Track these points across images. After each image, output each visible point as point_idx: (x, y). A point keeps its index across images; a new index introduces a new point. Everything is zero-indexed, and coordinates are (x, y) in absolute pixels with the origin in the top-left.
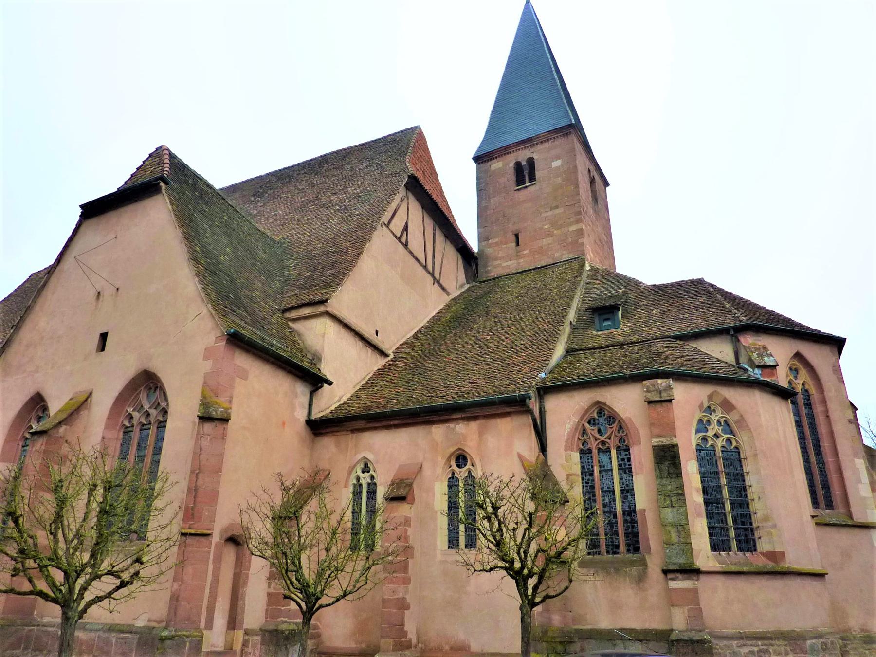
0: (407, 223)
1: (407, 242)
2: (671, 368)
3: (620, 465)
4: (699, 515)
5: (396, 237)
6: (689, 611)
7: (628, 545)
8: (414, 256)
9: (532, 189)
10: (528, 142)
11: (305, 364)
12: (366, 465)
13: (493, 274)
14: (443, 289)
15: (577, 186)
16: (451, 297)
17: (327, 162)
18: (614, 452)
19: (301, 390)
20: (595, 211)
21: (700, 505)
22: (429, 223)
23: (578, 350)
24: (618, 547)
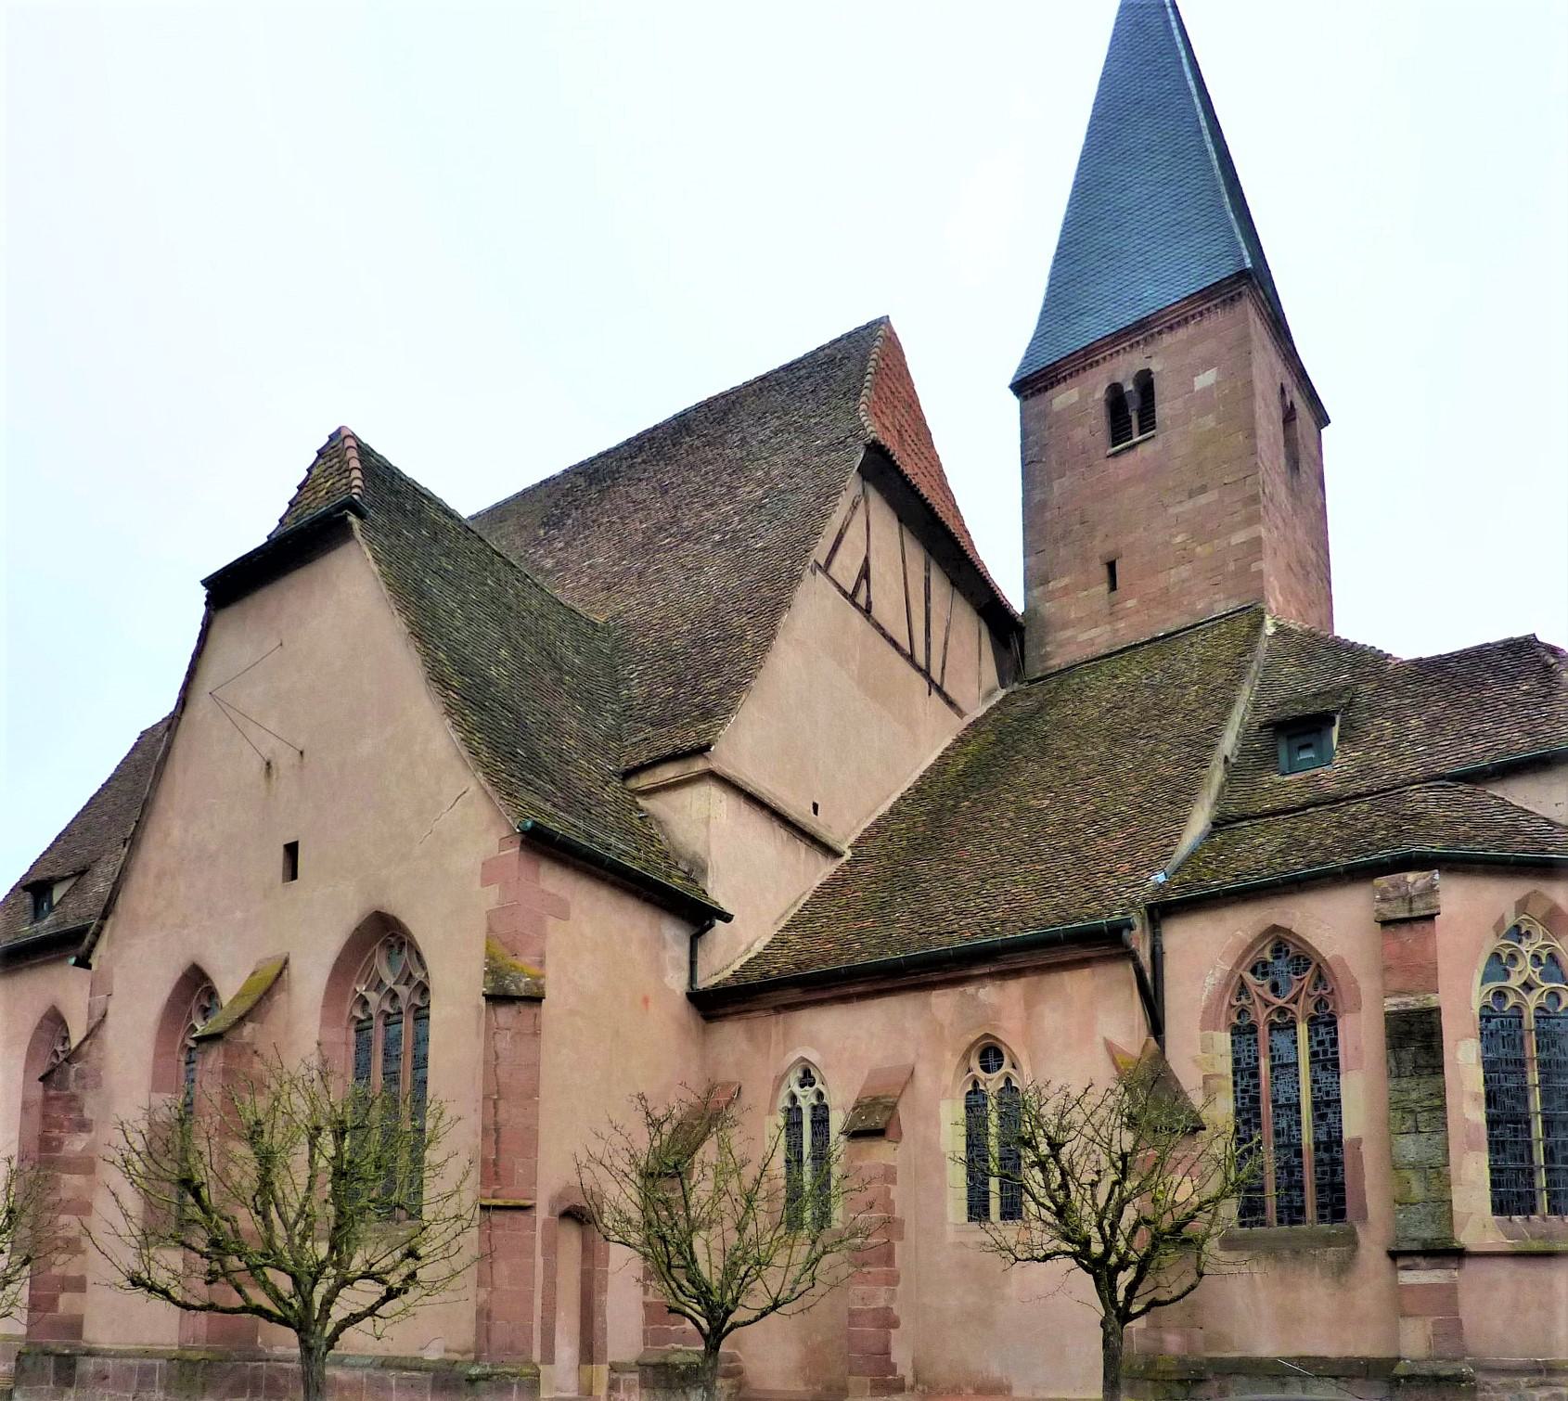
0: (866, 560)
1: (869, 603)
2: (1438, 848)
3: (1314, 1054)
4: (1472, 1146)
5: (845, 593)
6: (1434, 1324)
7: (1321, 1206)
8: (885, 635)
9: (1146, 450)
10: (1141, 331)
11: (676, 883)
12: (807, 1073)
14: (951, 703)
16: (969, 719)
18: (1302, 1029)
19: (673, 935)
21: (1477, 1126)
22: (916, 556)
24: (1301, 1210)
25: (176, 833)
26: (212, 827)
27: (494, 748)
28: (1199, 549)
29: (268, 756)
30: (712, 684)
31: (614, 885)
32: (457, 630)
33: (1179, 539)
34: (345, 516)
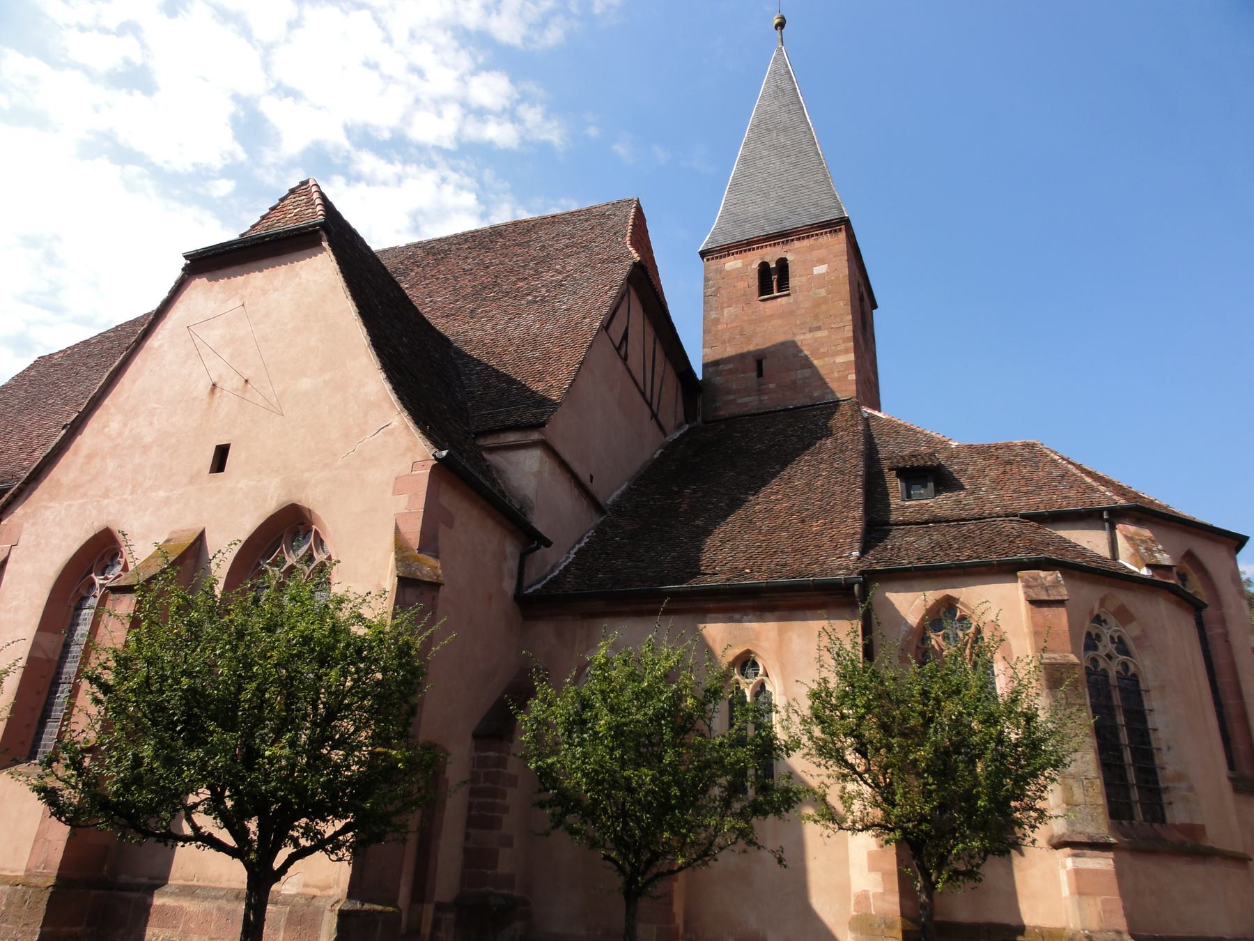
6: (1103, 902)
17: (501, 236)
22: (650, 331)
25: (115, 426)
26: (151, 424)
29: (215, 380)
31: (1209, 538)
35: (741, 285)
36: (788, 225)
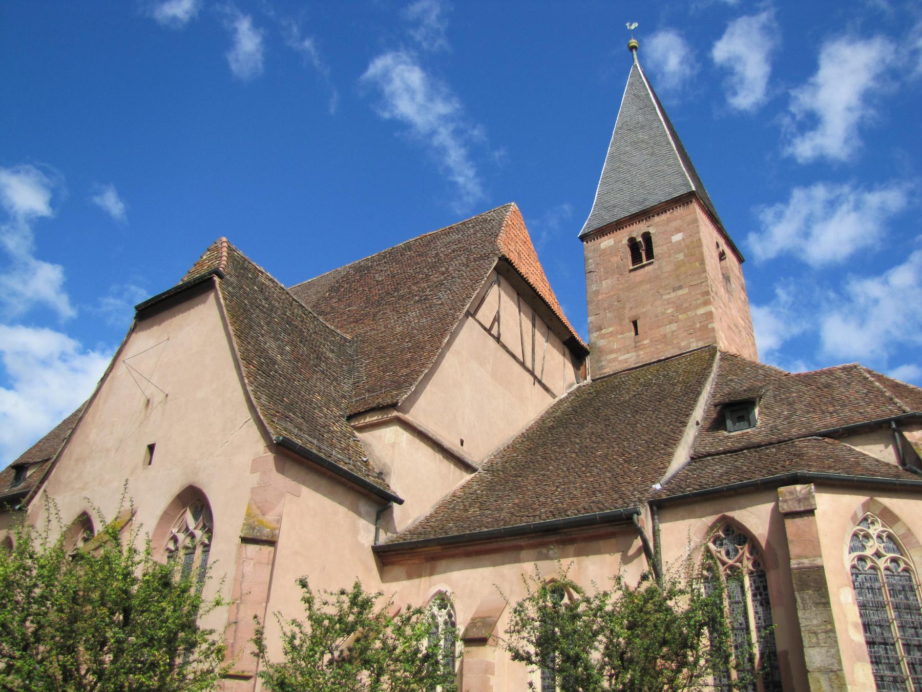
0: (498, 312)
1: (499, 334)
2: (813, 472)
5: (485, 329)
8: (508, 351)
10: (645, 214)
11: (370, 480)
13: (608, 371)
14: (547, 389)
15: (702, 262)
20: (728, 291)
23: (706, 456)
27: (271, 397)
28: (680, 316)
30: (405, 371)
31: (330, 478)
32: (263, 336)
33: (669, 311)
34: (212, 278)
35: (615, 260)
36: (649, 204)
